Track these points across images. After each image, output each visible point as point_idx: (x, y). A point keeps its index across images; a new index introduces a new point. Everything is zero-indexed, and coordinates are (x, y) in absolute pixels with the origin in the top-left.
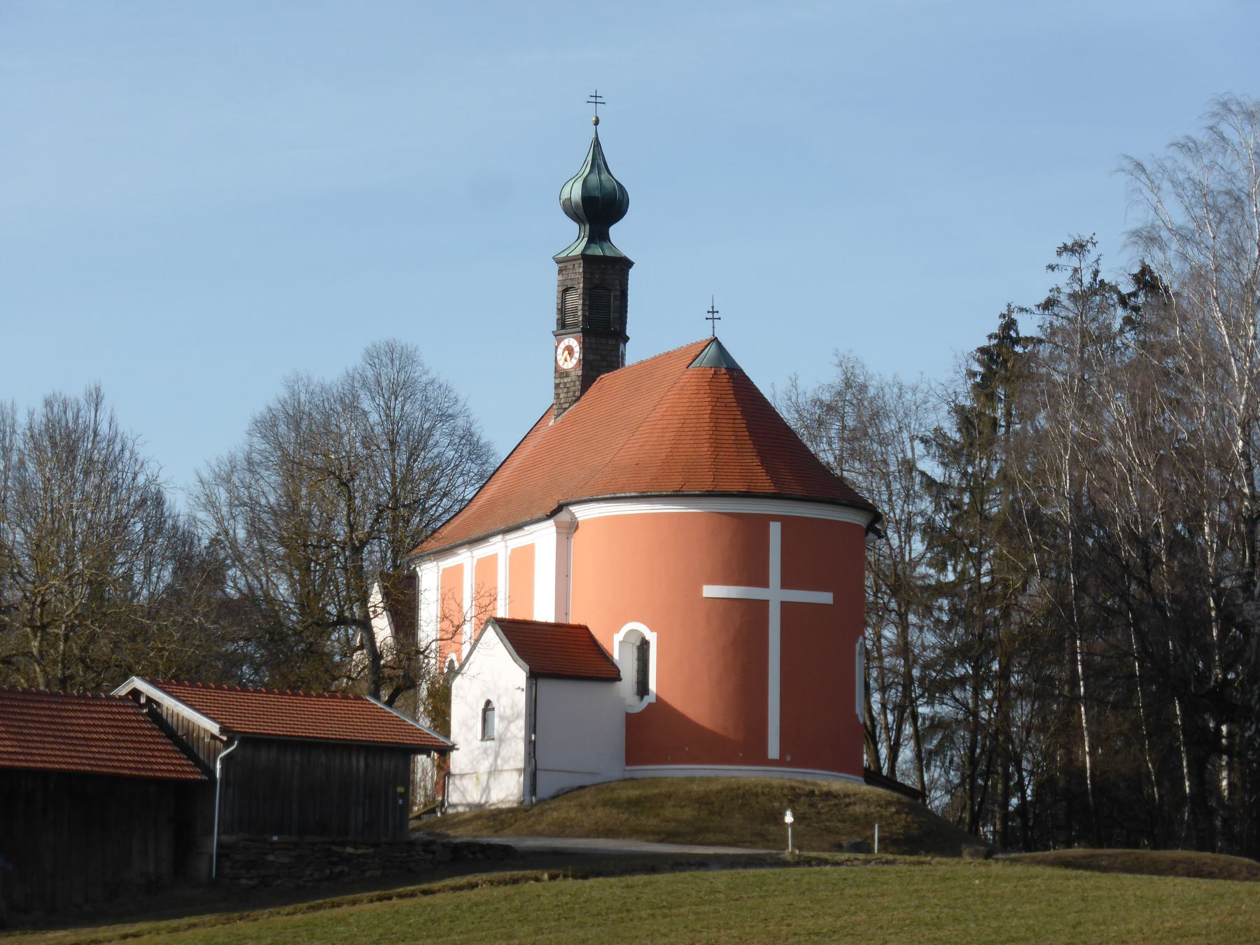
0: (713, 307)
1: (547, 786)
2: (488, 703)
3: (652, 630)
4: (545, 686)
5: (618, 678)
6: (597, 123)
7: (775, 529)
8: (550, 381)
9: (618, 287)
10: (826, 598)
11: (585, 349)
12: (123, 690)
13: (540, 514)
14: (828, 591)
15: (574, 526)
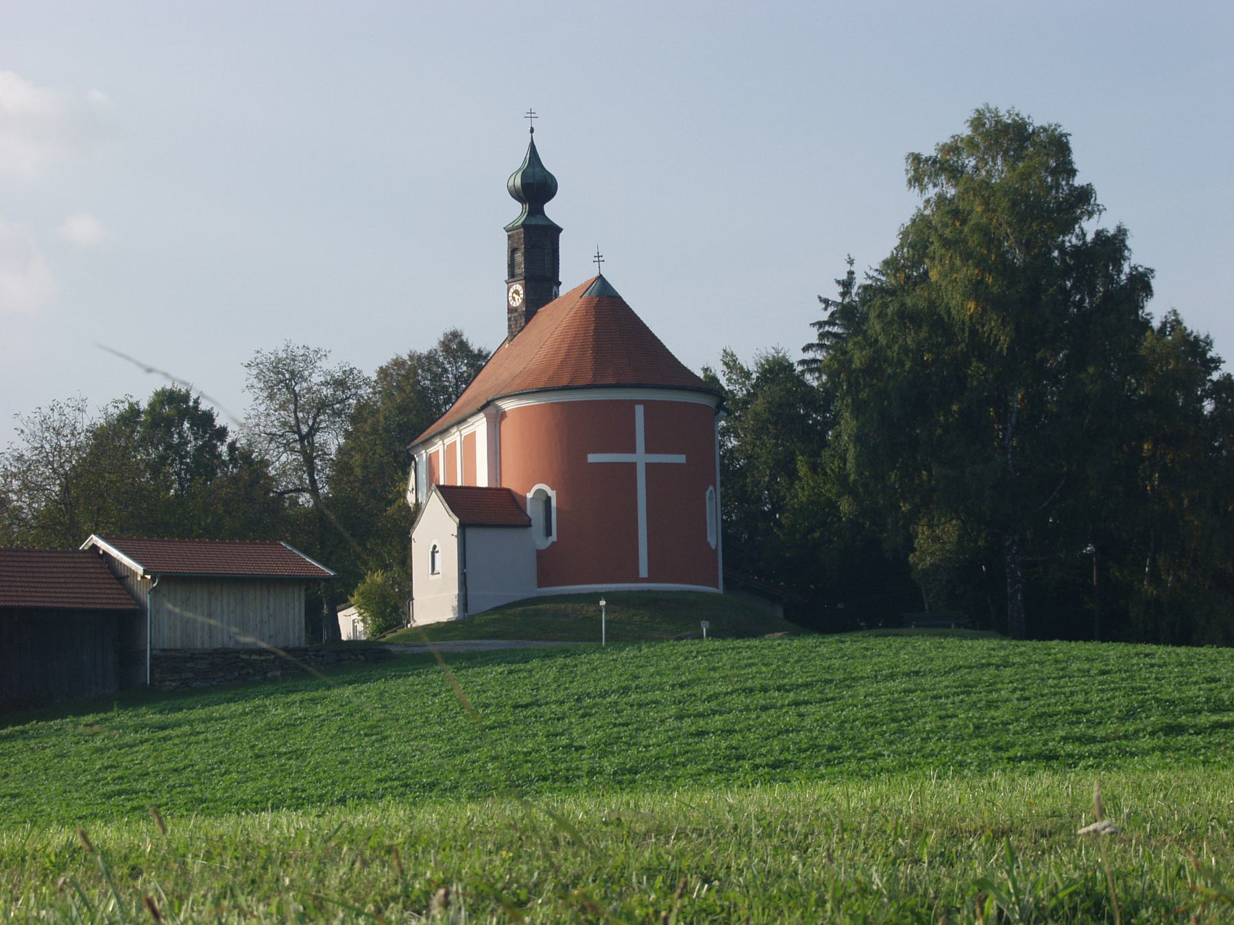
1: (483, 602)
2: (435, 547)
3: (552, 490)
4: (470, 532)
6: (532, 131)
7: (639, 410)
8: (505, 316)
10: (680, 459)
12: (84, 546)
13: (475, 410)
14: (682, 454)
15: (503, 415)
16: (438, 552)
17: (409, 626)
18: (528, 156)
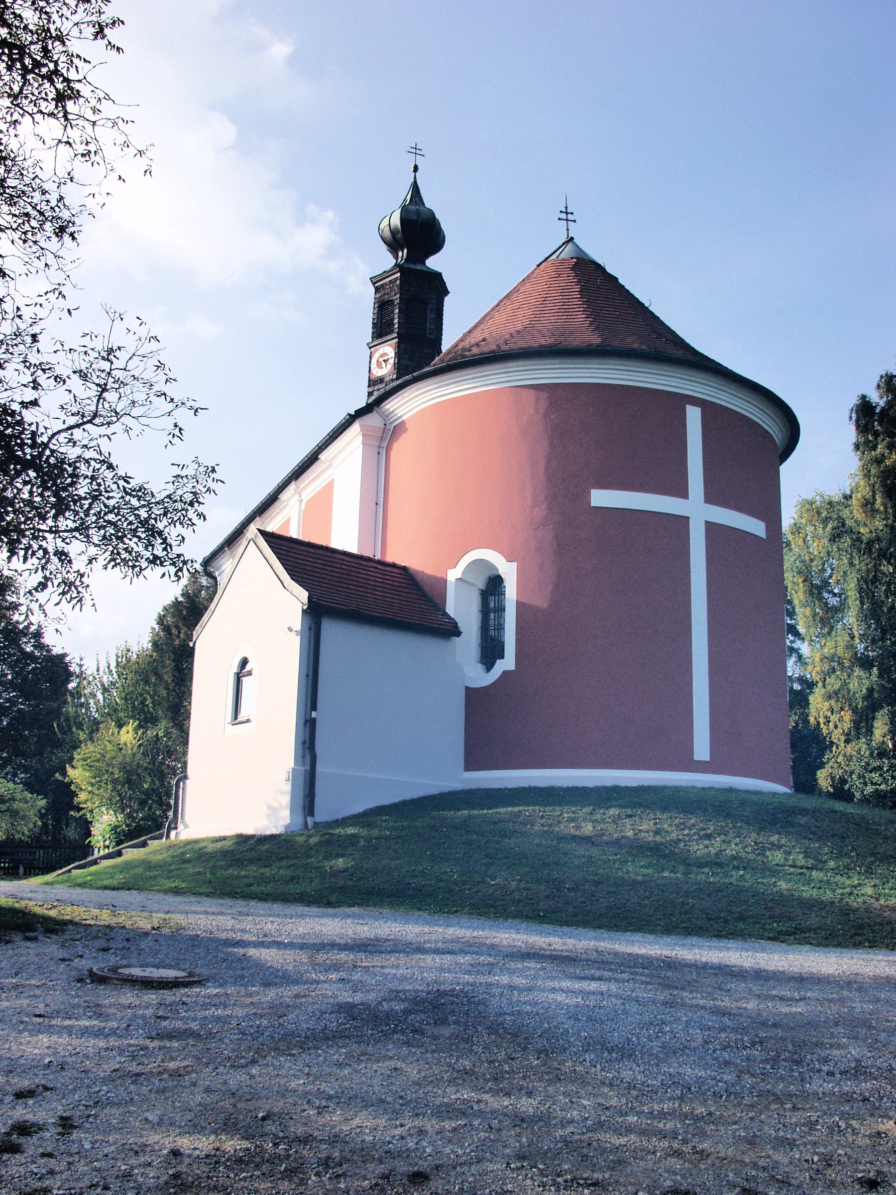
0: (566, 208)
2: (244, 662)
3: (510, 560)
4: (332, 630)
5: (458, 633)
6: (416, 169)
9: (435, 301)
11: (399, 355)
16: (250, 673)
17: (173, 834)
18: (409, 196)
